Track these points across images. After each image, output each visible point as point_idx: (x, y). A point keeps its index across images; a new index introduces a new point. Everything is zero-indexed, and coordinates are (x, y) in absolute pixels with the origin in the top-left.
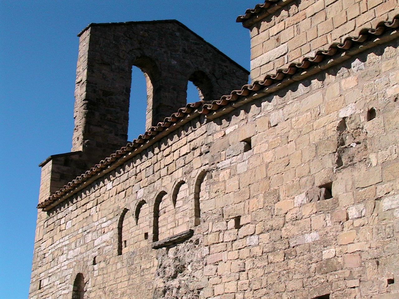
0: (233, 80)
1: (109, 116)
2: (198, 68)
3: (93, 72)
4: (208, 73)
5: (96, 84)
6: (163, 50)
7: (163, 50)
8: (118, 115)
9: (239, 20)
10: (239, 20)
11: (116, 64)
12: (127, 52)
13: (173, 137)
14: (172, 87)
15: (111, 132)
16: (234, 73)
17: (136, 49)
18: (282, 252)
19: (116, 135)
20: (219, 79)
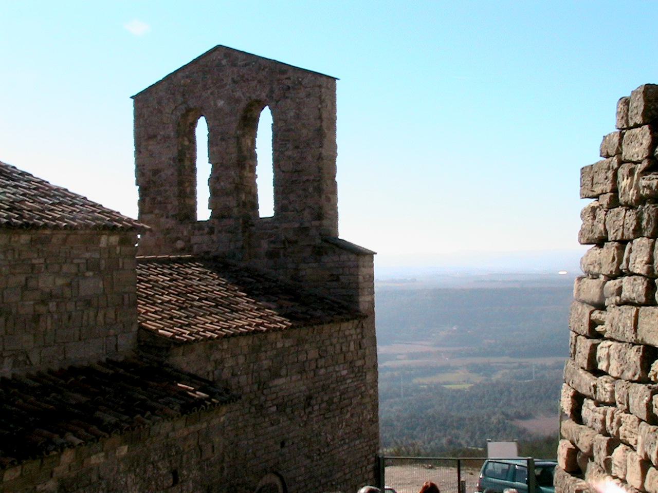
0: (298, 93)
1: (159, 198)
2: (250, 97)
3: (140, 152)
4: (265, 98)
5: (144, 165)
6: (209, 92)
7: (209, 92)
8: (168, 193)
9: (376, 253)
10: (376, 253)
11: (161, 133)
12: (170, 112)
13: (604, 244)
14: (219, 137)
15: (162, 216)
16: (300, 83)
17: (181, 104)
18: (370, 404)
19: (167, 217)
20: (279, 101)
